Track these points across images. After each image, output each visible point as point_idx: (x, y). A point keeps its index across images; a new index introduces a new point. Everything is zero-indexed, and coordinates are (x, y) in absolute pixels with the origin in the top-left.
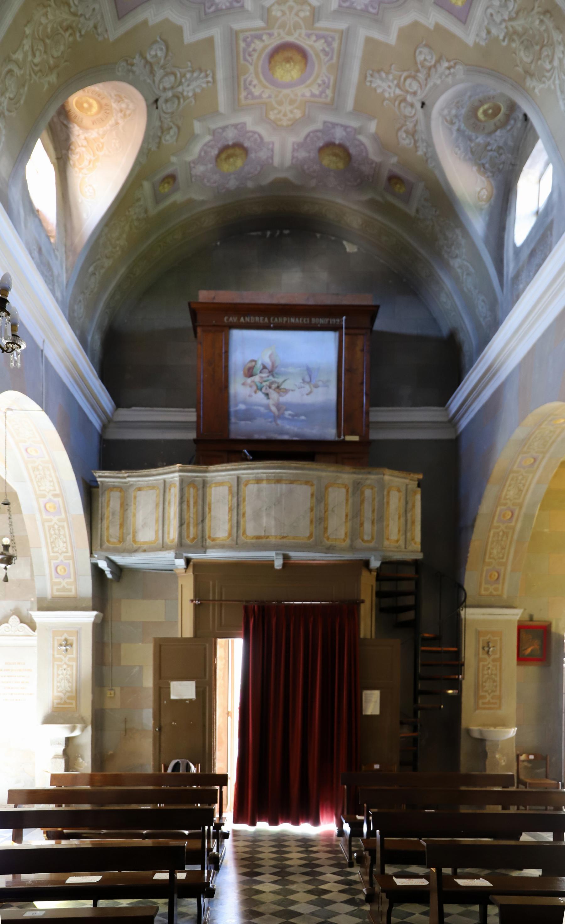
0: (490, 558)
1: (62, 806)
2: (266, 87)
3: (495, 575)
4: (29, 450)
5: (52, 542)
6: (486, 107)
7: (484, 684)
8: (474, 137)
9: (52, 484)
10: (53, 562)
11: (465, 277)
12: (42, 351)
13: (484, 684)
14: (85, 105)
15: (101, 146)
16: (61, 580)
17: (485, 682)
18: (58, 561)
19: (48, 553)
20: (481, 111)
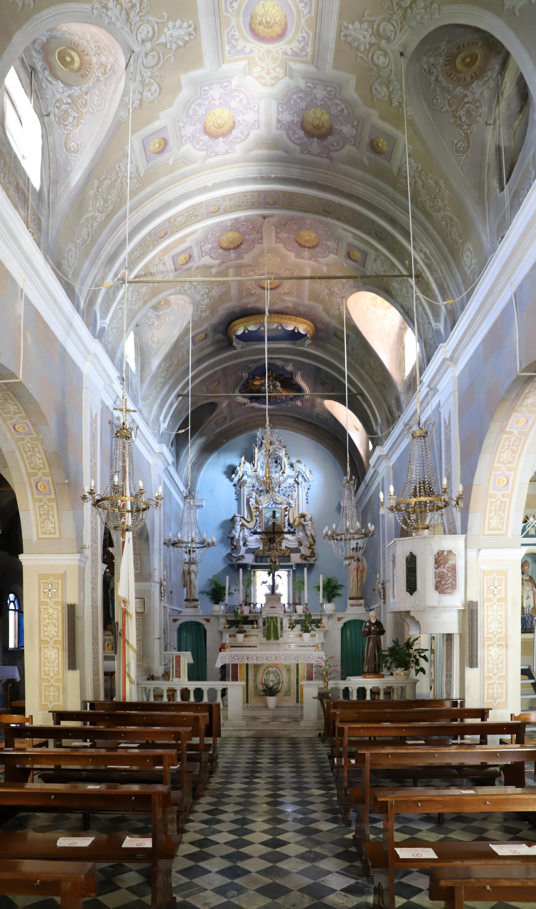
0: (499, 462)
1: (46, 744)
2: (248, 42)
3: (504, 481)
4: (17, 427)
5: (42, 522)
6: (463, 55)
7: (489, 626)
8: (451, 89)
9: (53, 525)
10: (32, 479)
11: (449, 229)
12: (22, 290)
13: (489, 626)
14: (68, 59)
15: (84, 102)
16: (42, 496)
17: (491, 623)
18: (38, 478)
19: (27, 470)
20: (459, 60)
